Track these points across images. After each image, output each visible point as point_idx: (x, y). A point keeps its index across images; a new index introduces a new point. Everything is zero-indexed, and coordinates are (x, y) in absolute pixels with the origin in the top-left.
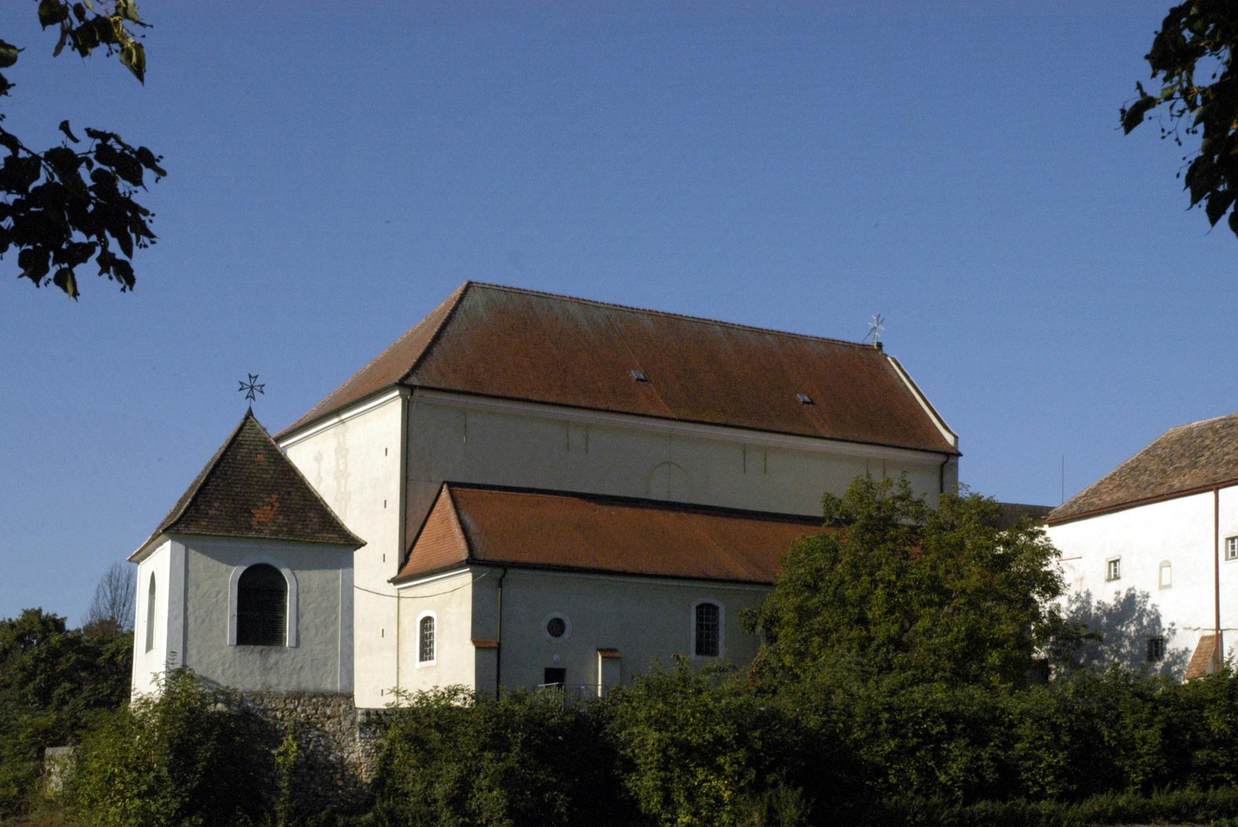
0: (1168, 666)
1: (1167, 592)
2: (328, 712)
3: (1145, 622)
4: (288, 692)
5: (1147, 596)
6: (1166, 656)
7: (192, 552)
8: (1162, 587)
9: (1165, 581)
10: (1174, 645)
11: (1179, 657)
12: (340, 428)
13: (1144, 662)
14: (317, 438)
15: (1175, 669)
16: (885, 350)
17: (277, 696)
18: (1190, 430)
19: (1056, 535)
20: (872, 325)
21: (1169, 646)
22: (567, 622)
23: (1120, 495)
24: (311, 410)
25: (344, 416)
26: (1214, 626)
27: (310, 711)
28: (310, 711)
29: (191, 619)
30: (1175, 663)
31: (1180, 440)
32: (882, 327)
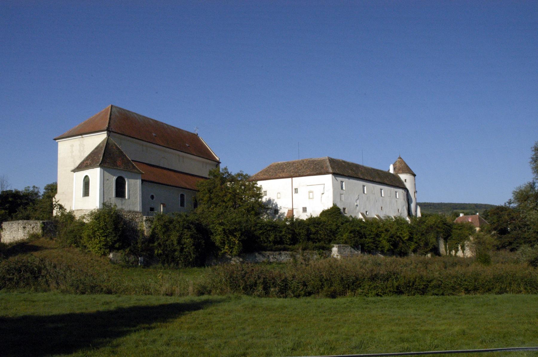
0: (279, 216)
1: (279, 199)
2: (137, 216)
3: (274, 206)
4: (127, 211)
5: (274, 200)
6: (279, 214)
7: (105, 172)
8: (278, 198)
9: (279, 197)
10: (281, 211)
11: (282, 214)
12: (82, 139)
13: (273, 215)
14: (72, 140)
15: (281, 217)
16: (198, 135)
17: (125, 212)
18: (279, 164)
19: (260, 183)
20: (195, 129)
21: (280, 212)
22: (155, 196)
23: (265, 176)
24: (66, 133)
25: (83, 136)
26: (292, 208)
27: (132, 216)
28: (132, 216)
29: (105, 190)
30: (281, 215)
31: (277, 165)
32: (198, 130)
